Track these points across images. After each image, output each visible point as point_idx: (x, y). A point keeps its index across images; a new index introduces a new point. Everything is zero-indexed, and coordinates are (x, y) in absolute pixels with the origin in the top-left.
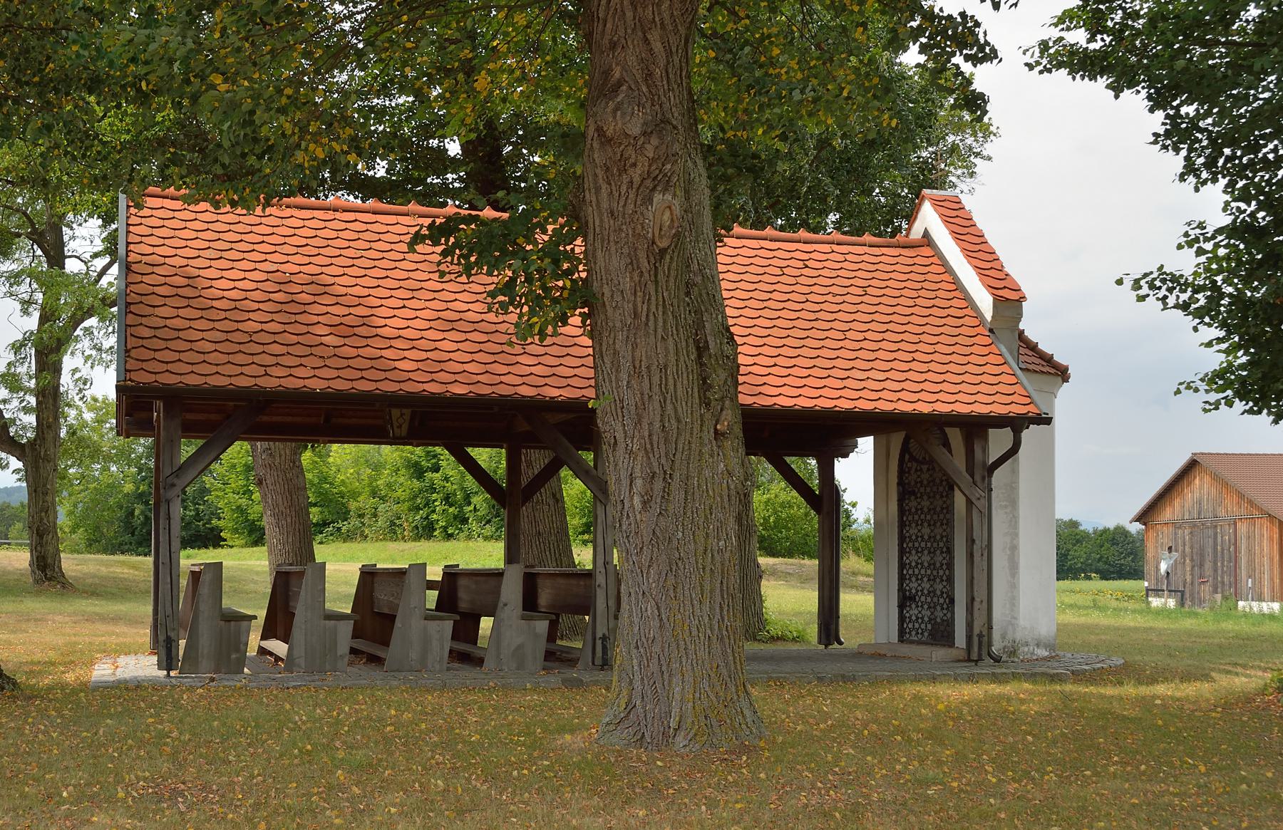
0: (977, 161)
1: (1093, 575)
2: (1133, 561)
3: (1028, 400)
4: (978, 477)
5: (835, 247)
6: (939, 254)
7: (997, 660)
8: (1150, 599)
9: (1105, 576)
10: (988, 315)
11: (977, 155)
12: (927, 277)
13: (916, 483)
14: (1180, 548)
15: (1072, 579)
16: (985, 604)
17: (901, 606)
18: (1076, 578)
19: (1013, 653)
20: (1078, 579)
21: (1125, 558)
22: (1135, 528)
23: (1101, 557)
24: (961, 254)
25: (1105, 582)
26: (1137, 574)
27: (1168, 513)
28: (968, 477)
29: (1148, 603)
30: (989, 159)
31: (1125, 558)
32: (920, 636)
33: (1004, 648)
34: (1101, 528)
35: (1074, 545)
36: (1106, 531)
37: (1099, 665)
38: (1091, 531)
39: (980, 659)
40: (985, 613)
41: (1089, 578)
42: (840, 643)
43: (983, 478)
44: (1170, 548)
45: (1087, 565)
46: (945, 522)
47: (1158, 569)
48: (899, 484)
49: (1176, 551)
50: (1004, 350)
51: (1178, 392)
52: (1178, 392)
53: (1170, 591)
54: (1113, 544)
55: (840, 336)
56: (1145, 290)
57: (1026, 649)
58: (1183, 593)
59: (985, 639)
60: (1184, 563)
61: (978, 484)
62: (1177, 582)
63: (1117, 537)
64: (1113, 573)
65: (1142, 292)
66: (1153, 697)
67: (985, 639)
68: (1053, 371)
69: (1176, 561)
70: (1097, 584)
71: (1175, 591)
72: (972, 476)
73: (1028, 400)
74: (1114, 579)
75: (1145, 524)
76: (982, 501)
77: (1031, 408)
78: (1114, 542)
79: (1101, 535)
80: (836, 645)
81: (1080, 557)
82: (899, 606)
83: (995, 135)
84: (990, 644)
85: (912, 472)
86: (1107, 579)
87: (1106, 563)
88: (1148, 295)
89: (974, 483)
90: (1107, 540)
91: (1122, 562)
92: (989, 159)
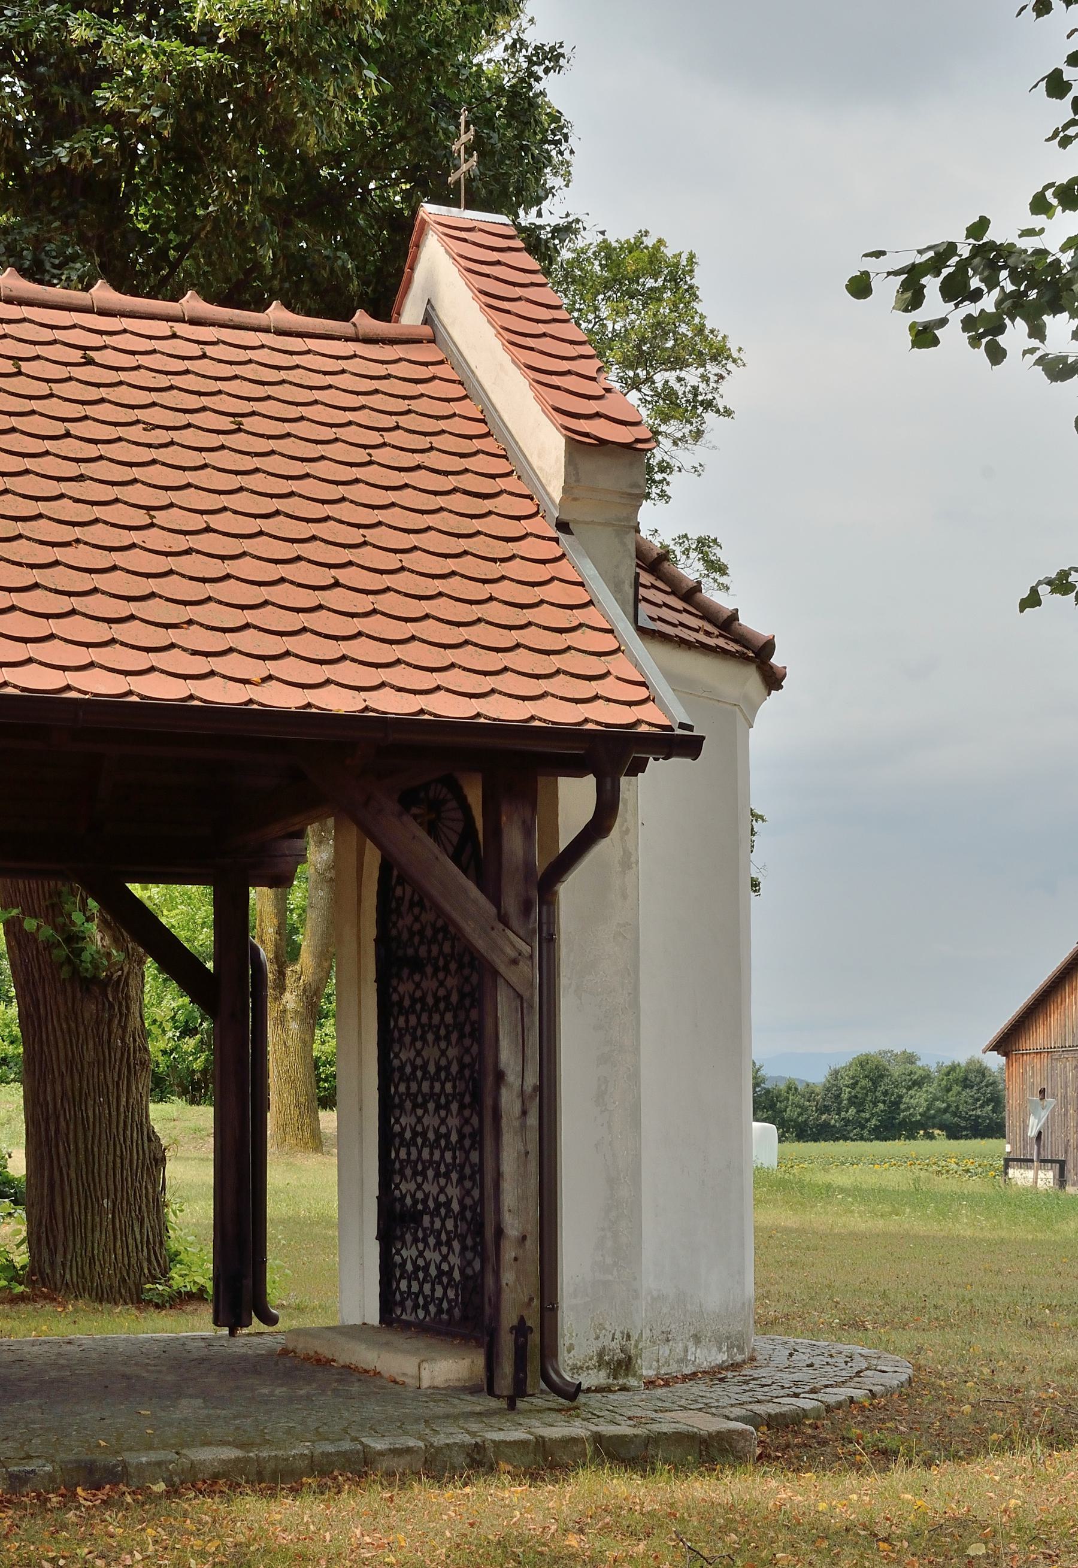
0: (710, 416)
1: (937, 1132)
2: (994, 1111)
3: (641, 693)
4: (511, 904)
5: (182, 329)
6: (451, 358)
7: (571, 1393)
8: (1011, 1171)
9: (954, 1133)
10: (555, 488)
11: (708, 405)
12: (414, 405)
13: (412, 934)
14: (1060, 1092)
15: (908, 1138)
16: (532, 1246)
17: (387, 1237)
18: (911, 1137)
19: (623, 1365)
20: (915, 1138)
21: (982, 1106)
22: (995, 1061)
23: (949, 1106)
24: (476, 306)
25: (953, 1142)
26: (996, 1130)
27: (1039, 1037)
28: (482, 899)
29: (1007, 1181)
30: (728, 413)
31: (982, 1106)
32: (421, 1314)
33: (601, 1354)
34: (948, 1063)
35: (909, 1088)
36: (953, 1068)
37: (843, 1393)
38: (933, 1068)
39: (520, 1390)
40: (534, 1268)
41: (931, 1137)
42: (270, 1319)
43: (526, 908)
44: (1042, 1092)
45: (929, 1118)
46: (467, 1029)
47: (1025, 1127)
48: (378, 941)
49: (1054, 1096)
50: (589, 571)
51: (1032, 600)
52: (1032, 600)
53: (1042, 1161)
54: (965, 1087)
55: (140, 518)
56: (934, 305)
57: (665, 1351)
58: (1062, 1164)
59: (535, 1338)
60: (1066, 1114)
61: (515, 922)
62: (1054, 1149)
63: (971, 1076)
64: (965, 1128)
65: (922, 315)
66: (962, 1523)
67: (535, 1338)
68: (732, 647)
69: (1053, 1111)
70: (942, 1145)
71: (1052, 1161)
72: (496, 900)
73: (641, 693)
74: (967, 1137)
75: (1006, 1054)
76: (524, 967)
77: (651, 714)
78: (966, 1083)
79: (948, 1074)
80: (257, 1325)
81: (918, 1105)
82: (379, 1237)
83: (734, 361)
84: (549, 1349)
85: (404, 908)
86: (956, 1138)
87: (955, 1114)
88: (943, 322)
89: (503, 919)
90: (956, 1081)
91: (979, 1112)
92: (728, 413)
